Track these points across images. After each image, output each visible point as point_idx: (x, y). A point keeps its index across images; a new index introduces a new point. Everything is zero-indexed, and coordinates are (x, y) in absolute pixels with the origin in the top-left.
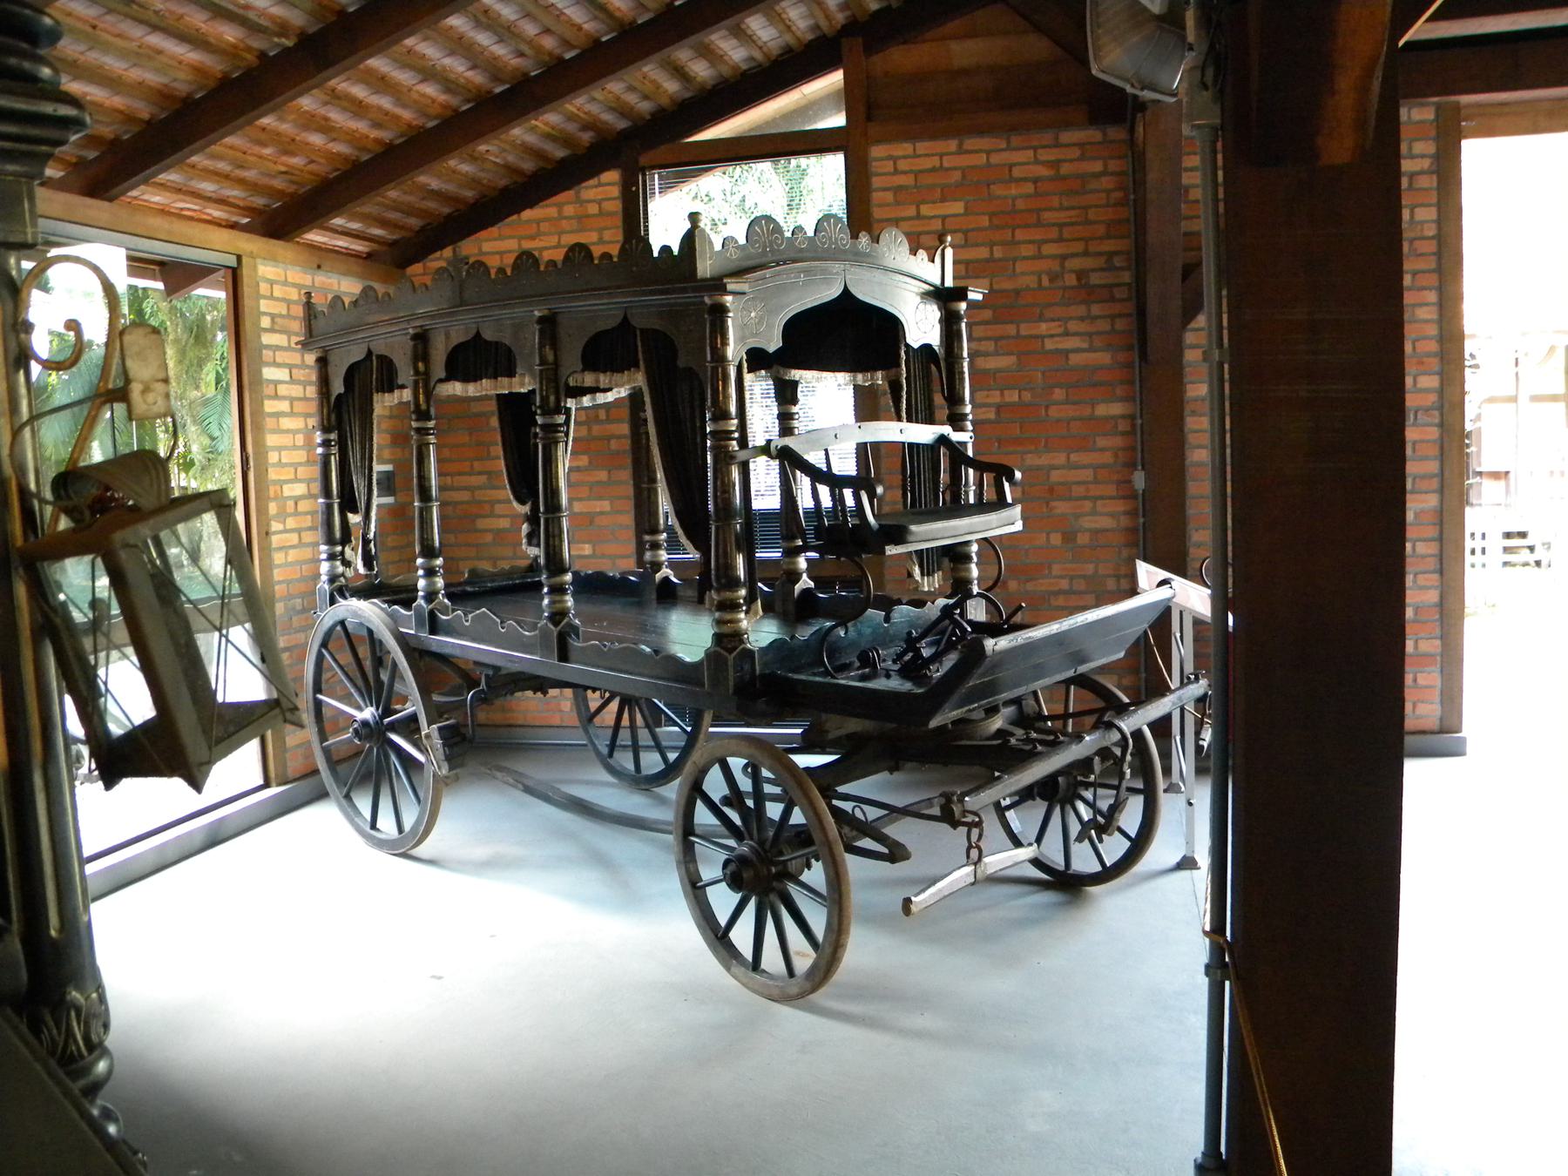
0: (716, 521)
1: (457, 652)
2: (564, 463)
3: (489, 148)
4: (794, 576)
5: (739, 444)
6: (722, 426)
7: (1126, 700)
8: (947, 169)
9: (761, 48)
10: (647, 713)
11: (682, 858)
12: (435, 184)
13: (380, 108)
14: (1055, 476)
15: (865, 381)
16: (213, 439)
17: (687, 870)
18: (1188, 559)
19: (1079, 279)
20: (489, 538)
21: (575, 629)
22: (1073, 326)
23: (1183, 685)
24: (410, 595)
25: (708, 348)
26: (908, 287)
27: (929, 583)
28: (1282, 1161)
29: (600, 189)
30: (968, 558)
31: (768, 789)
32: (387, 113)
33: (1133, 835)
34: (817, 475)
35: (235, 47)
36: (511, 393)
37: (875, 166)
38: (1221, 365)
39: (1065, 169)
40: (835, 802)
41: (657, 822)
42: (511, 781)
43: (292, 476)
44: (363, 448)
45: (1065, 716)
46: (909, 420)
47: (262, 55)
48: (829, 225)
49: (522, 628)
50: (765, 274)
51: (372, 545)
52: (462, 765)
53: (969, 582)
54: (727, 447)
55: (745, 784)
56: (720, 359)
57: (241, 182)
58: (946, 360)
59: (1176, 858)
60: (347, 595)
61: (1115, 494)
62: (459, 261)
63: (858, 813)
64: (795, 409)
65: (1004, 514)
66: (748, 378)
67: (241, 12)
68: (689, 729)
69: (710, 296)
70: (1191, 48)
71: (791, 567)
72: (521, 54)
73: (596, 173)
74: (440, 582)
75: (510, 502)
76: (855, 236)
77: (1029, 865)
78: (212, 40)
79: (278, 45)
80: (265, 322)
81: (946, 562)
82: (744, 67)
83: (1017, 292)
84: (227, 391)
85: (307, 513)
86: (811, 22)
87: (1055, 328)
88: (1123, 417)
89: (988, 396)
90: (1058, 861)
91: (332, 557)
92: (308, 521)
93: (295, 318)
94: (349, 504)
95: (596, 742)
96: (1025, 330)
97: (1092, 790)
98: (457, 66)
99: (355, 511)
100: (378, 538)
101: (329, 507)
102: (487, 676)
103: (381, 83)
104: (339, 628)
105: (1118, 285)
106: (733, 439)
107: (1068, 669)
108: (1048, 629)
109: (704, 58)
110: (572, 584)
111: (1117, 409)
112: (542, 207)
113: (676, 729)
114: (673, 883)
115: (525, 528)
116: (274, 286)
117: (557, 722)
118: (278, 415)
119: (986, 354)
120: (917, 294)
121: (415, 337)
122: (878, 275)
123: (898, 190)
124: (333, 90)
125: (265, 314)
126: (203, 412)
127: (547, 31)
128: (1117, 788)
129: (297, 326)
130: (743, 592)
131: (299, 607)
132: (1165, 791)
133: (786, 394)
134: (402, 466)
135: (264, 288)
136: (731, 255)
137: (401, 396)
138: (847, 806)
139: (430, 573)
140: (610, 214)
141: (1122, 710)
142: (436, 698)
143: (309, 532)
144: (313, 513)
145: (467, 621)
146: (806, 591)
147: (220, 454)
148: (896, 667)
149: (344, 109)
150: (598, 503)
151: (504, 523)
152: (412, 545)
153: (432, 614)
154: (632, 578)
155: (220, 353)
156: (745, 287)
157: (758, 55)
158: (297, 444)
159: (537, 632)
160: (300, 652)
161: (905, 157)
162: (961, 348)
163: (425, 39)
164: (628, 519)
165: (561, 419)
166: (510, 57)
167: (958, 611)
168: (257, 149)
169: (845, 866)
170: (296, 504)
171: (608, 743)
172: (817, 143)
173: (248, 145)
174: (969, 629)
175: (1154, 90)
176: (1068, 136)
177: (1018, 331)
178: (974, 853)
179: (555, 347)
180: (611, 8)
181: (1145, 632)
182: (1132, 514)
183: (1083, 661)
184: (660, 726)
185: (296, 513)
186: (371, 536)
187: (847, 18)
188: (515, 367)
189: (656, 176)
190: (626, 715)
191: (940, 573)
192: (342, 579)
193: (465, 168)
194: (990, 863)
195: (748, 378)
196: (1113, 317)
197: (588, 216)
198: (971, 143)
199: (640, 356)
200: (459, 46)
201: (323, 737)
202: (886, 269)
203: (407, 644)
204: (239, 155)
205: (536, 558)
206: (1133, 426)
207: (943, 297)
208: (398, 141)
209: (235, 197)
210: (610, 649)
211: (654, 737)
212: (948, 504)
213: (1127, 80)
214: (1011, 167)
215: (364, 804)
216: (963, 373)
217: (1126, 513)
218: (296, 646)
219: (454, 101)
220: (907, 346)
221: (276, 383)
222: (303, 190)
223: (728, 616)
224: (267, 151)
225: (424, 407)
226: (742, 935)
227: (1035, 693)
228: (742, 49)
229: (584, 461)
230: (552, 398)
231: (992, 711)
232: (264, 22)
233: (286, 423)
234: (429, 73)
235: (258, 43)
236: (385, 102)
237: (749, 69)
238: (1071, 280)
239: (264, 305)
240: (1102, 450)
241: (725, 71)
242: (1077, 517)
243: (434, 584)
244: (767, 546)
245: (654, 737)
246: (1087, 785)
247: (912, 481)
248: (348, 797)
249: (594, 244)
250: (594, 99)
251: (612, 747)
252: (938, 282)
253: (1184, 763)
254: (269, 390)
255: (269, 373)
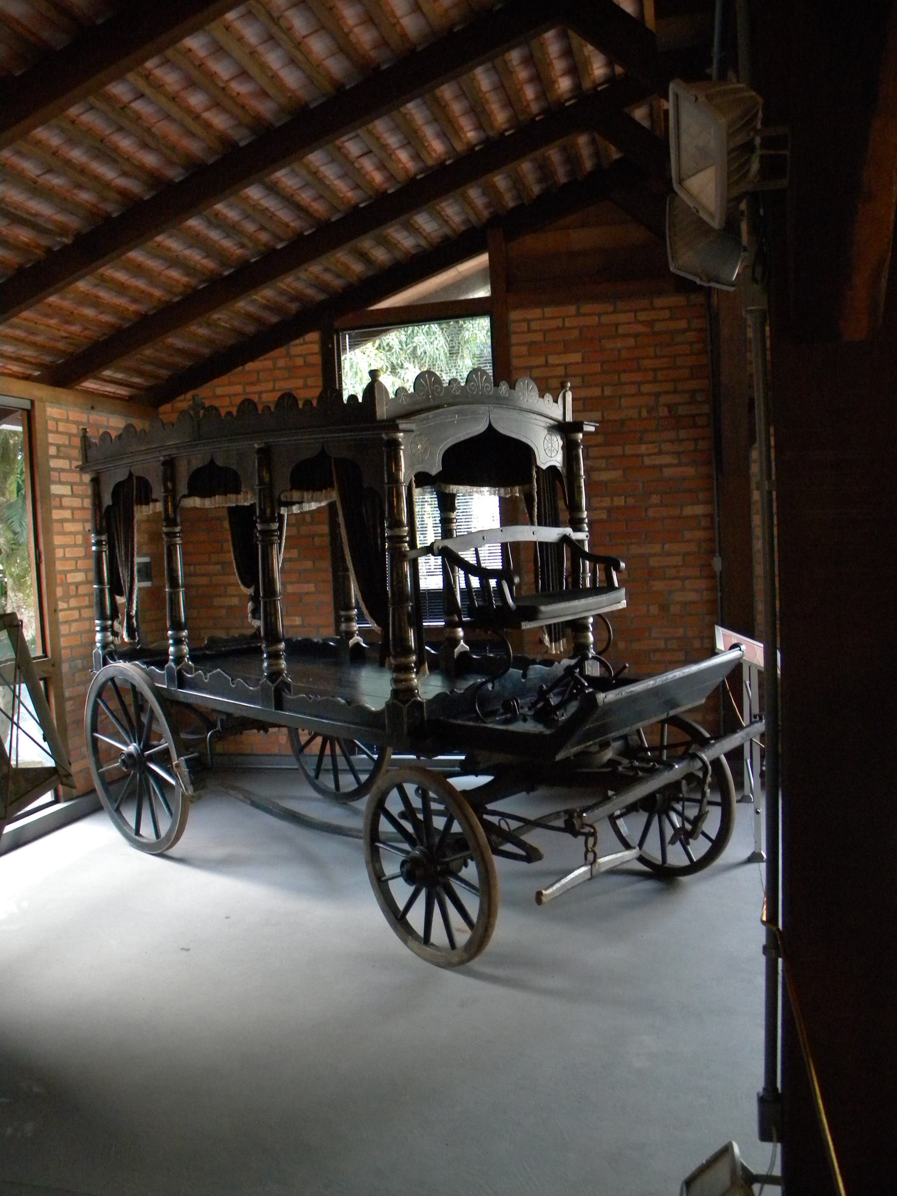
0: (392, 605)
1: (200, 702)
2: (278, 562)
3: (221, 316)
4: (455, 642)
5: (409, 545)
6: (397, 532)
7: (708, 735)
8: (569, 328)
9: (425, 238)
10: (343, 745)
11: (370, 859)
12: (179, 343)
13: (137, 288)
14: (653, 562)
15: (506, 494)
16: (15, 533)
17: (374, 867)
18: (755, 624)
19: (670, 412)
20: (223, 612)
21: (287, 685)
22: (665, 447)
23: (751, 723)
24: (163, 658)
25: (386, 473)
26: (538, 422)
27: (555, 648)
28: (820, 1101)
29: (305, 346)
30: (587, 628)
31: (434, 806)
32: (143, 292)
33: (713, 837)
34: (470, 569)
35: (27, 244)
36: (237, 506)
37: (513, 327)
38: (770, 493)
39: (659, 326)
40: (485, 817)
41: (351, 830)
42: (241, 797)
43: (74, 568)
44: (126, 546)
45: (661, 748)
46: (540, 524)
47: (48, 250)
48: (477, 376)
49: (247, 683)
50: (428, 416)
51: (134, 620)
52: (204, 787)
53: (586, 647)
54: (400, 548)
55: (417, 803)
56: (394, 480)
57: (34, 344)
58: (567, 477)
59: (747, 853)
60: (116, 658)
61: (698, 574)
62: (197, 405)
63: (504, 825)
64: (453, 515)
65: (612, 595)
66: (416, 491)
67: (32, 219)
68: (376, 757)
69: (386, 434)
70: (745, 250)
71: (453, 635)
72: (243, 246)
73: (299, 334)
74: (185, 649)
75: (239, 586)
76: (496, 384)
77: (637, 861)
78: (11, 240)
79: (59, 243)
80: (52, 451)
81: (569, 631)
82: (413, 252)
83: (623, 422)
84: (25, 498)
85: (85, 595)
86: (463, 217)
87: (652, 449)
88: (705, 516)
89: (601, 501)
90: (657, 857)
91: (104, 629)
92: (86, 601)
93: (75, 447)
94: (117, 589)
95: (306, 768)
96: (629, 450)
97: (681, 803)
98: (195, 256)
99: (121, 594)
100: (139, 614)
101: (101, 591)
102: (222, 720)
103: (138, 270)
104: (110, 683)
105: (701, 415)
106: (406, 542)
107: (663, 713)
108: (646, 684)
109: (383, 246)
110: (284, 651)
111: (699, 510)
112: (261, 361)
113: (365, 756)
114: (363, 876)
115: (250, 605)
116: (59, 423)
117: (276, 751)
118: (63, 521)
119: (598, 470)
120: (545, 428)
121: (164, 464)
122: (514, 414)
123: (531, 344)
124: (102, 275)
125: (52, 444)
126: (7, 513)
127: (262, 228)
128: (700, 802)
129: (76, 453)
130: (414, 658)
131: (80, 666)
132: (738, 801)
133: (447, 504)
134: (156, 558)
135: (51, 425)
136: (402, 401)
137: (155, 507)
138: (494, 819)
139: (178, 642)
140: (314, 365)
141: (704, 743)
142: (183, 736)
143: (86, 610)
144: (90, 595)
145: (206, 679)
146: (463, 654)
147: (20, 545)
148: (531, 713)
149: (111, 289)
150: (306, 585)
151: (235, 601)
152: (163, 619)
153: (180, 672)
154: (332, 644)
155: (20, 469)
156: (412, 426)
157: (423, 243)
158: (78, 543)
159: (259, 687)
160: (80, 700)
161: (536, 319)
162: (579, 469)
163: (171, 236)
164: (328, 598)
165: (275, 526)
166: (235, 248)
167: (578, 670)
168: (46, 320)
169: (492, 866)
170: (77, 588)
171: (315, 767)
172: (473, 309)
173: (40, 317)
174: (586, 684)
175: (718, 282)
176: (659, 302)
177: (624, 451)
178: (590, 856)
179: (270, 471)
180: (311, 210)
181: (723, 682)
182: (712, 589)
183: (673, 708)
184: (354, 754)
185: (77, 595)
186: (134, 613)
187: (491, 213)
188: (240, 487)
189: (347, 336)
190: (328, 746)
191: (565, 640)
192: (112, 646)
193: (203, 331)
194: (603, 863)
195: (416, 491)
196: (695, 440)
197: (295, 367)
198: (586, 308)
199: (334, 478)
200: (197, 241)
201: (99, 765)
202: (522, 410)
203: (162, 696)
204: (32, 324)
205: (259, 628)
206: (712, 522)
207: (563, 429)
208: (151, 313)
209: (29, 356)
210: (314, 700)
211: (349, 762)
212: (570, 587)
213: (696, 275)
214: (617, 326)
215: (130, 816)
216: (580, 487)
217: (707, 589)
218: (79, 696)
219: (193, 282)
220: (538, 468)
221: (61, 497)
222: (81, 350)
223: (402, 676)
224: (53, 322)
225: (171, 515)
226: (416, 918)
227: (638, 731)
228: (411, 238)
229: (294, 553)
230: (268, 511)
231: (605, 745)
232: (49, 226)
233: (69, 527)
234: (175, 262)
235: (45, 241)
236: (141, 284)
237: (418, 253)
238: (663, 412)
239: (51, 438)
240: (689, 541)
241: (398, 255)
242: (670, 592)
243: (181, 650)
244: (434, 616)
245: (349, 762)
246: (678, 800)
247: (542, 572)
248: (118, 810)
249: (299, 388)
250: (299, 278)
251: (318, 771)
252: (560, 418)
253: (752, 780)
254: (55, 502)
255: (56, 489)
